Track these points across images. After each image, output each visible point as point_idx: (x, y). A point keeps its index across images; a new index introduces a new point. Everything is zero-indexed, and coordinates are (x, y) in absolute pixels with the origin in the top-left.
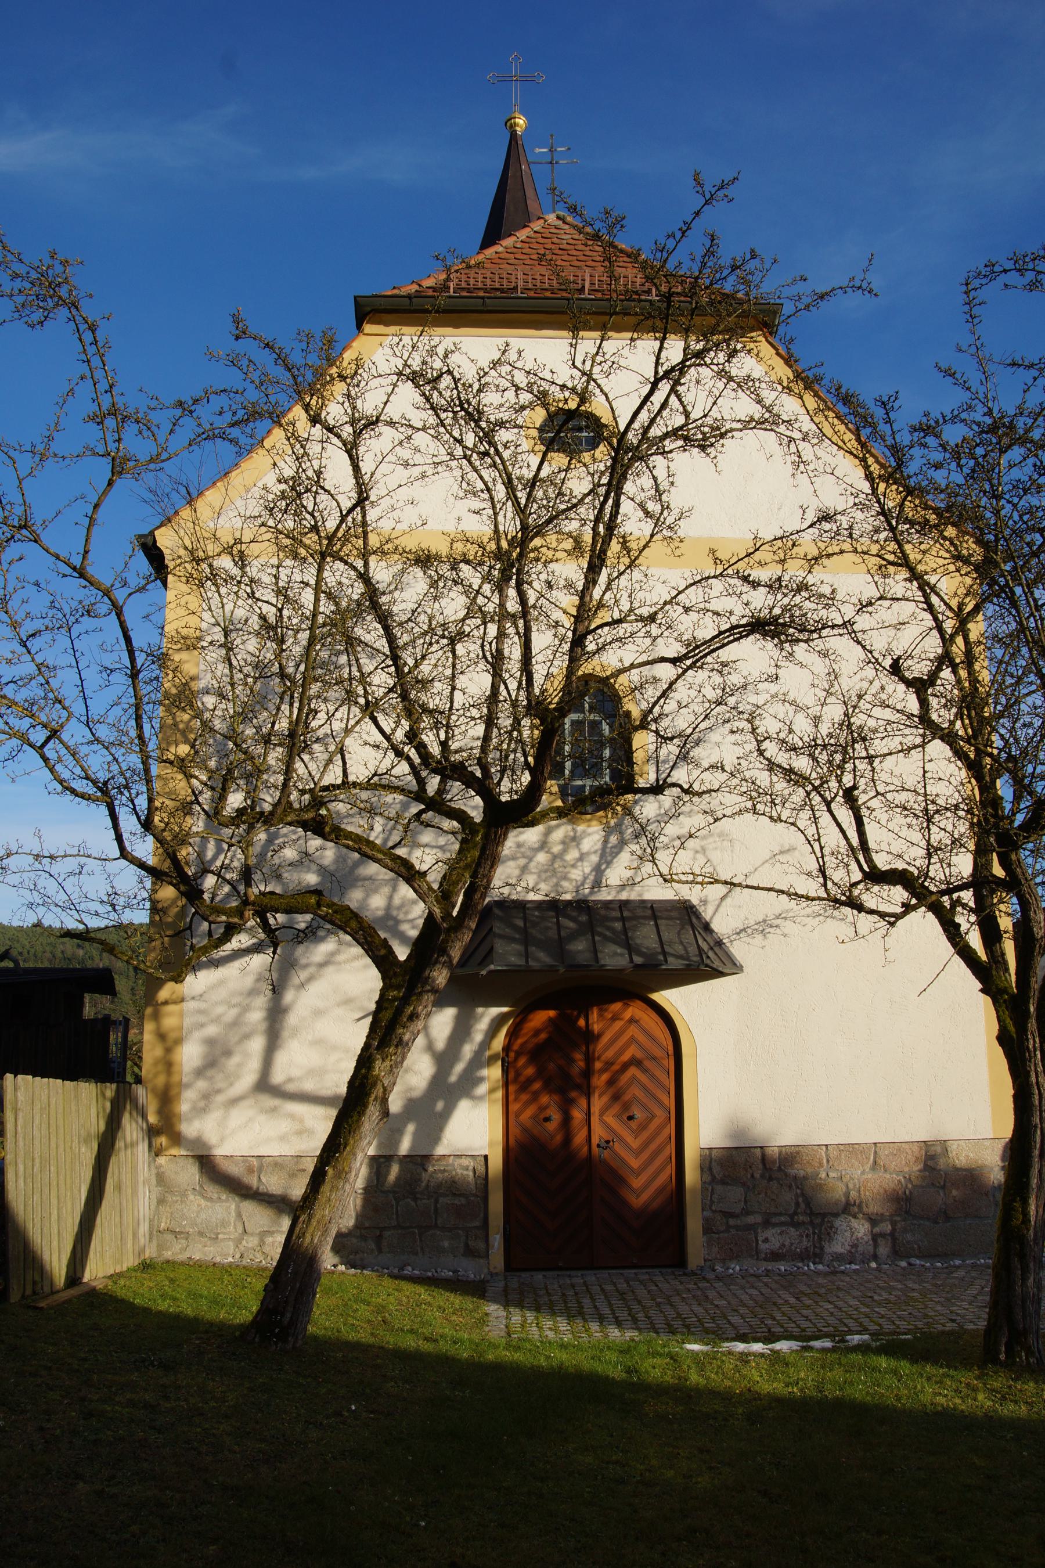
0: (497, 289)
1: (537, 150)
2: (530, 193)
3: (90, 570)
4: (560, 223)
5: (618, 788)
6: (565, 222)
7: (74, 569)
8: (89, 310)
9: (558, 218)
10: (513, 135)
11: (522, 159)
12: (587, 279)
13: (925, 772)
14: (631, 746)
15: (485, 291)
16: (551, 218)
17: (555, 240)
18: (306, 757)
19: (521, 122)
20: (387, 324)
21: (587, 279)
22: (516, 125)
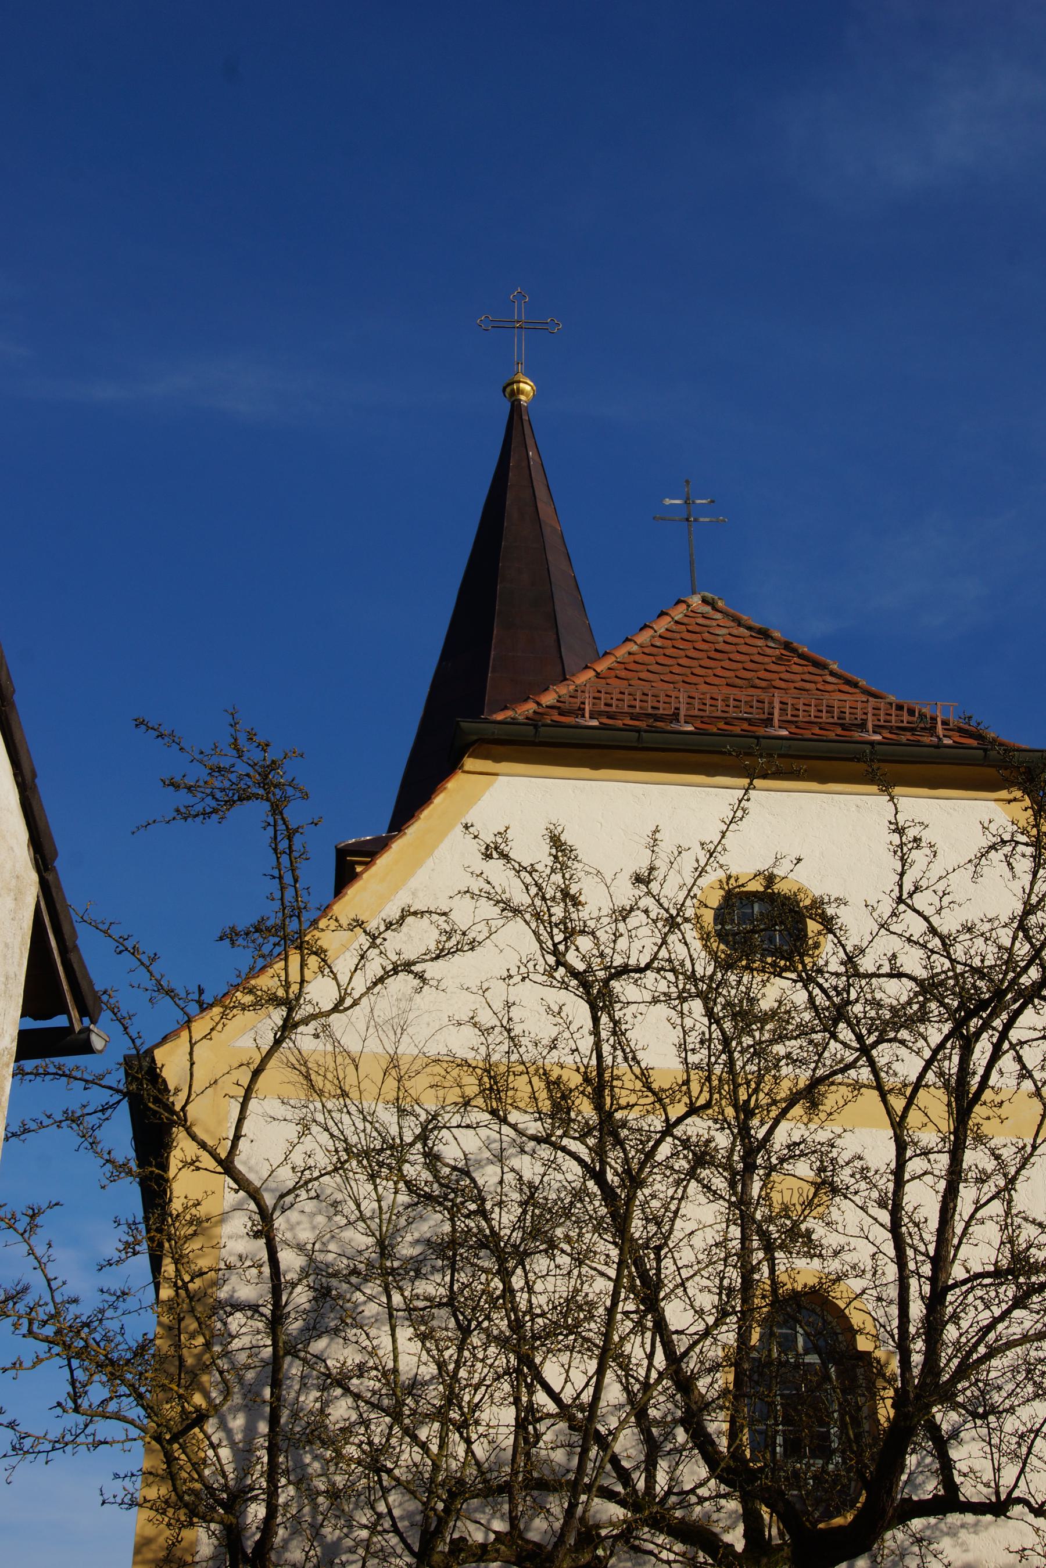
0: (649, 716)
1: (668, 501)
2: (541, 493)
3: (239, 1164)
4: (707, 609)
5: (728, 1469)
6: (715, 609)
7: (220, 1162)
8: (294, 814)
9: (705, 601)
10: (516, 407)
11: (530, 442)
12: (777, 705)
13: (49, 1281)
14: (935, 1424)
15: (633, 717)
16: (695, 601)
17: (706, 636)
18: (135, 1403)
19: (527, 387)
20: (497, 759)
21: (777, 705)
22: (520, 391)
